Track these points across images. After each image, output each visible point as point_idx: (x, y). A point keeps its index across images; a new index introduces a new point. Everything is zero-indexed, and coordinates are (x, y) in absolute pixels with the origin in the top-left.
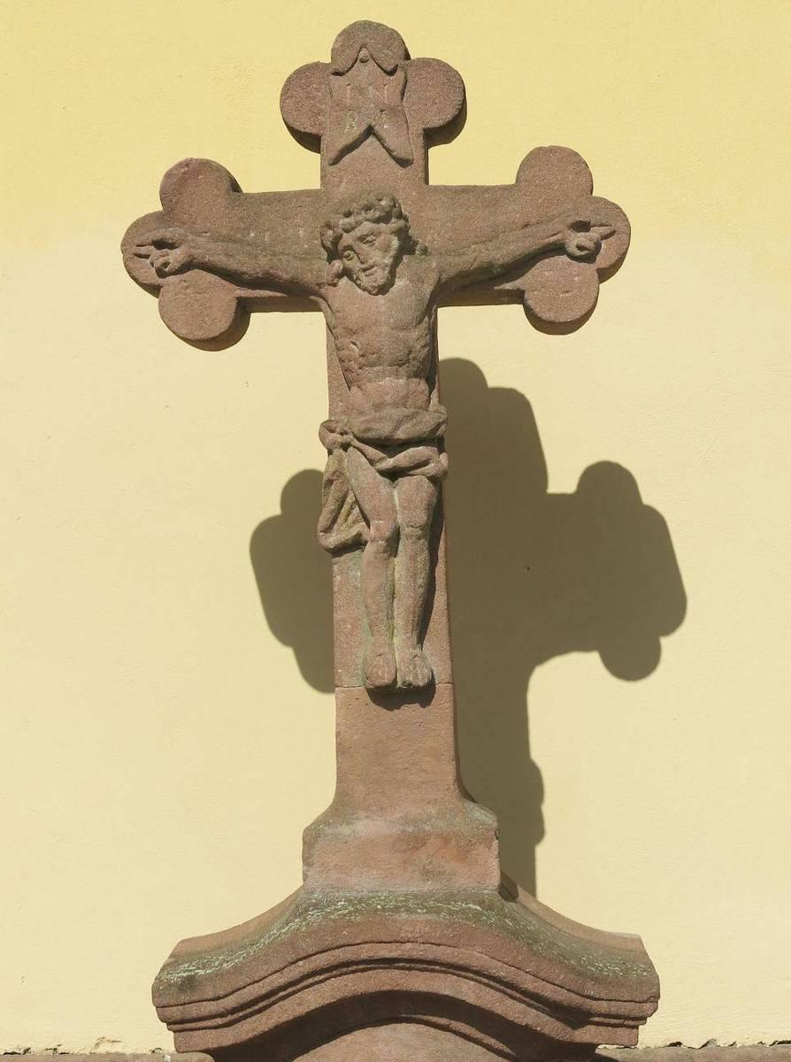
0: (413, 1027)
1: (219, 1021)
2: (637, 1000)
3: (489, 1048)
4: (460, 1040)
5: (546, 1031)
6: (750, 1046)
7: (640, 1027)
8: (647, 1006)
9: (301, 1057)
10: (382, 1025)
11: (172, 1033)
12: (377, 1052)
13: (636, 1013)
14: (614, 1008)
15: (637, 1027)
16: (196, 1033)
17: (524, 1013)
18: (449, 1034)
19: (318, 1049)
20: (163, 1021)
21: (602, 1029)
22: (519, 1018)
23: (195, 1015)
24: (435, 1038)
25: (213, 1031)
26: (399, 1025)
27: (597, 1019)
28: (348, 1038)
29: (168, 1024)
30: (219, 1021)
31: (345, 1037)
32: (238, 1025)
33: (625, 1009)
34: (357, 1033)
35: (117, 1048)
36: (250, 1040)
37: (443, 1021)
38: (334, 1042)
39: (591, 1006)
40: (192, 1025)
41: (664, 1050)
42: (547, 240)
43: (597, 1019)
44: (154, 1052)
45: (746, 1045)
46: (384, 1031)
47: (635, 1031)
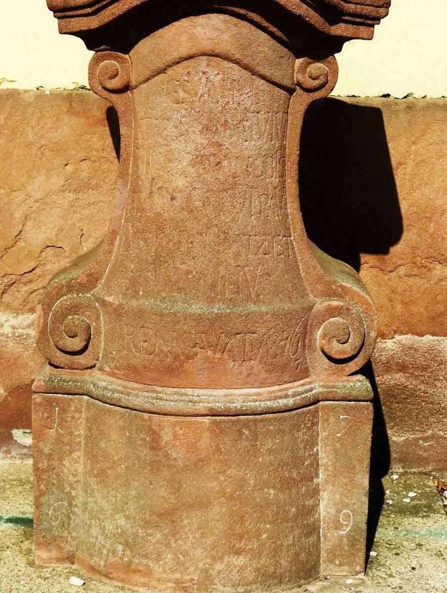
0: (222, 17)
1: (89, 10)
2: (375, 4)
3: (272, 35)
4: (253, 28)
5: (312, 22)
6: (436, 98)
7: (376, 26)
8: (382, 10)
9: (144, 40)
10: (201, 15)
11: (56, 19)
12: (196, 33)
13: (374, 14)
14: (359, 9)
15: (373, 26)
16: (73, 20)
17: (298, 6)
18: (245, 23)
19: (156, 32)
20: (51, 9)
21: (350, 26)
22: (295, 9)
23: (72, 5)
24: (236, 25)
25: (85, 18)
26: (212, 15)
27: (347, 18)
28: (177, 24)
29: (54, 13)
30: (89, 10)
31: (175, 23)
32: (102, 13)
33: (367, 10)
34: (183, 20)
35: (11, 86)
36: (110, 22)
37: (242, 11)
38: (167, 27)
39: (344, 7)
40: (71, 13)
41: (378, 99)
42: (269, 403)
43: (347, 18)
44: (38, 89)
45: (433, 97)
46: (201, 19)
47: (372, 29)
